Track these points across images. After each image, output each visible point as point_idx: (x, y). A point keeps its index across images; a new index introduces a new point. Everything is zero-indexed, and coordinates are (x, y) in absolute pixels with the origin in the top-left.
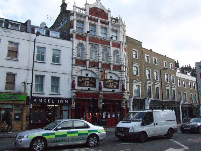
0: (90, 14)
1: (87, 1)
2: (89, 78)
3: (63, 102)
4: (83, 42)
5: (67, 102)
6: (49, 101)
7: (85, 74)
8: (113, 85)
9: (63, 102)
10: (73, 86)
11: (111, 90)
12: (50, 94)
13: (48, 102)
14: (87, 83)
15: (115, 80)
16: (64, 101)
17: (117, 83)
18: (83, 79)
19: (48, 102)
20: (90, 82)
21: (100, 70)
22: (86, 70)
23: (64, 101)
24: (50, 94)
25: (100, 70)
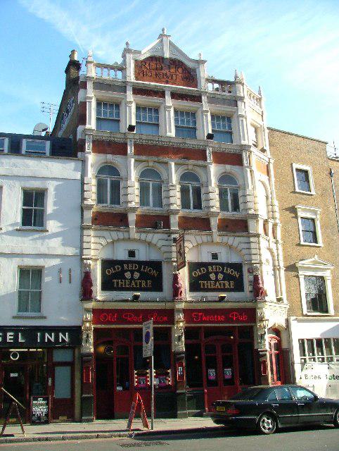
0: (137, 78)
1: (127, 44)
3: (52, 339)
4: (117, 160)
5: (67, 339)
6: (8, 337)
8: (224, 279)
9: (52, 339)
10: (87, 294)
11: (128, 295)
12: (14, 317)
13: (8, 341)
14: (132, 278)
16: (57, 337)
19: (8, 341)
20: (144, 276)
21: (173, 236)
23: (57, 337)
24: (14, 317)
25: (173, 236)
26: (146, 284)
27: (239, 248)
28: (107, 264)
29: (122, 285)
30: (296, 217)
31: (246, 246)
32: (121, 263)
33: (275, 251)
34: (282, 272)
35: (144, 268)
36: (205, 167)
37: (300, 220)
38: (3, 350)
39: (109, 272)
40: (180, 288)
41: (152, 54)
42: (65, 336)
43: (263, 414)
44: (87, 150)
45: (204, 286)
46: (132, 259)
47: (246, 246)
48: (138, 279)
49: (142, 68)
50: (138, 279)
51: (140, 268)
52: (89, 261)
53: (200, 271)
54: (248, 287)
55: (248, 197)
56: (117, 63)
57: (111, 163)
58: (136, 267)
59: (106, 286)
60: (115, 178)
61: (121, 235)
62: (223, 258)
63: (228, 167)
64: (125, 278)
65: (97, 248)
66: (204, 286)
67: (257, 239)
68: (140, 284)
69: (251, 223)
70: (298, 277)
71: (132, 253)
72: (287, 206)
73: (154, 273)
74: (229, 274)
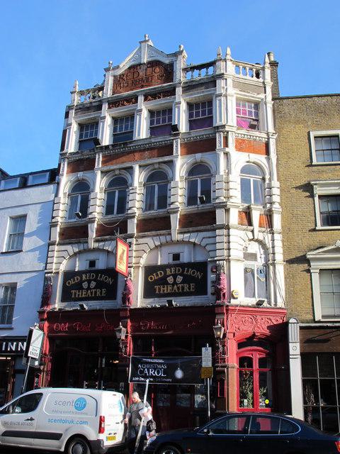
2: (183, 266)
7: (171, 256)
8: (183, 282)
15: (190, 265)
17: (198, 275)
18: (160, 274)
20: (187, 279)
22: (172, 243)
26: (101, 293)
27: (203, 244)
28: (150, 270)
29: (79, 295)
30: (312, 196)
31: (211, 241)
32: (163, 268)
33: (269, 245)
34: (280, 270)
35: (188, 271)
36: (171, 164)
37: (316, 199)
38: (103, 366)
39: (151, 278)
40: (221, 290)
41: (133, 63)
42: (13, 345)
43: (78, 443)
44: (217, 148)
45: (75, 295)
46: (93, 269)
47: (211, 241)
48: (94, 288)
49: (118, 81)
50: (94, 288)
51: (97, 277)
52: (221, 262)
53: (157, 275)
54: (210, 289)
55: (230, 183)
56: (97, 85)
57: (83, 179)
58: (179, 270)
59: (66, 297)
60: (205, 176)
61: (163, 238)
62: (185, 258)
63: (199, 156)
64: (168, 284)
65: (62, 262)
66: (75, 295)
67: (225, 232)
68: (183, 288)
69: (220, 214)
70: (308, 271)
71: (176, 257)
72: (297, 185)
73: (198, 275)
74: (103, 281)
